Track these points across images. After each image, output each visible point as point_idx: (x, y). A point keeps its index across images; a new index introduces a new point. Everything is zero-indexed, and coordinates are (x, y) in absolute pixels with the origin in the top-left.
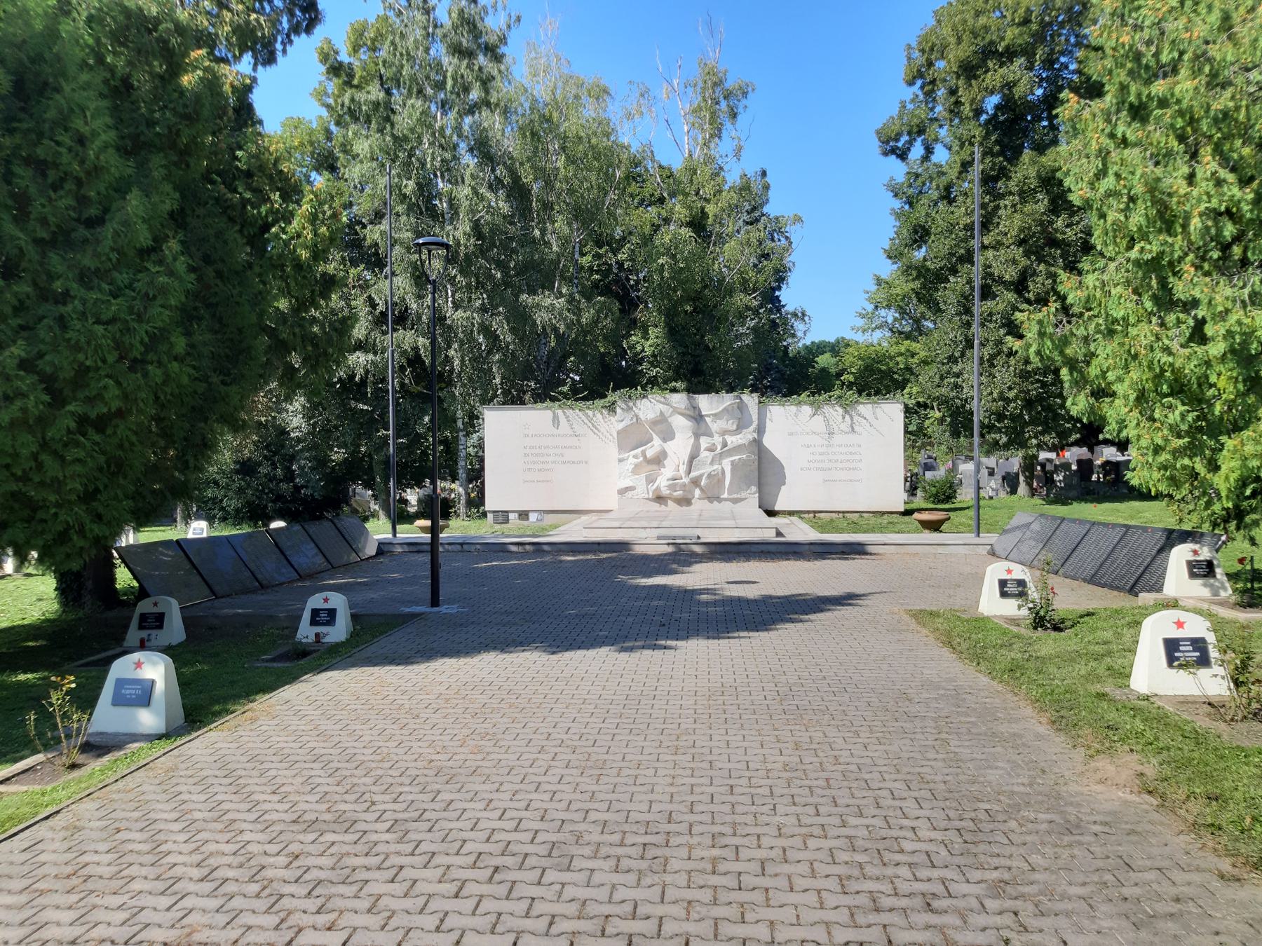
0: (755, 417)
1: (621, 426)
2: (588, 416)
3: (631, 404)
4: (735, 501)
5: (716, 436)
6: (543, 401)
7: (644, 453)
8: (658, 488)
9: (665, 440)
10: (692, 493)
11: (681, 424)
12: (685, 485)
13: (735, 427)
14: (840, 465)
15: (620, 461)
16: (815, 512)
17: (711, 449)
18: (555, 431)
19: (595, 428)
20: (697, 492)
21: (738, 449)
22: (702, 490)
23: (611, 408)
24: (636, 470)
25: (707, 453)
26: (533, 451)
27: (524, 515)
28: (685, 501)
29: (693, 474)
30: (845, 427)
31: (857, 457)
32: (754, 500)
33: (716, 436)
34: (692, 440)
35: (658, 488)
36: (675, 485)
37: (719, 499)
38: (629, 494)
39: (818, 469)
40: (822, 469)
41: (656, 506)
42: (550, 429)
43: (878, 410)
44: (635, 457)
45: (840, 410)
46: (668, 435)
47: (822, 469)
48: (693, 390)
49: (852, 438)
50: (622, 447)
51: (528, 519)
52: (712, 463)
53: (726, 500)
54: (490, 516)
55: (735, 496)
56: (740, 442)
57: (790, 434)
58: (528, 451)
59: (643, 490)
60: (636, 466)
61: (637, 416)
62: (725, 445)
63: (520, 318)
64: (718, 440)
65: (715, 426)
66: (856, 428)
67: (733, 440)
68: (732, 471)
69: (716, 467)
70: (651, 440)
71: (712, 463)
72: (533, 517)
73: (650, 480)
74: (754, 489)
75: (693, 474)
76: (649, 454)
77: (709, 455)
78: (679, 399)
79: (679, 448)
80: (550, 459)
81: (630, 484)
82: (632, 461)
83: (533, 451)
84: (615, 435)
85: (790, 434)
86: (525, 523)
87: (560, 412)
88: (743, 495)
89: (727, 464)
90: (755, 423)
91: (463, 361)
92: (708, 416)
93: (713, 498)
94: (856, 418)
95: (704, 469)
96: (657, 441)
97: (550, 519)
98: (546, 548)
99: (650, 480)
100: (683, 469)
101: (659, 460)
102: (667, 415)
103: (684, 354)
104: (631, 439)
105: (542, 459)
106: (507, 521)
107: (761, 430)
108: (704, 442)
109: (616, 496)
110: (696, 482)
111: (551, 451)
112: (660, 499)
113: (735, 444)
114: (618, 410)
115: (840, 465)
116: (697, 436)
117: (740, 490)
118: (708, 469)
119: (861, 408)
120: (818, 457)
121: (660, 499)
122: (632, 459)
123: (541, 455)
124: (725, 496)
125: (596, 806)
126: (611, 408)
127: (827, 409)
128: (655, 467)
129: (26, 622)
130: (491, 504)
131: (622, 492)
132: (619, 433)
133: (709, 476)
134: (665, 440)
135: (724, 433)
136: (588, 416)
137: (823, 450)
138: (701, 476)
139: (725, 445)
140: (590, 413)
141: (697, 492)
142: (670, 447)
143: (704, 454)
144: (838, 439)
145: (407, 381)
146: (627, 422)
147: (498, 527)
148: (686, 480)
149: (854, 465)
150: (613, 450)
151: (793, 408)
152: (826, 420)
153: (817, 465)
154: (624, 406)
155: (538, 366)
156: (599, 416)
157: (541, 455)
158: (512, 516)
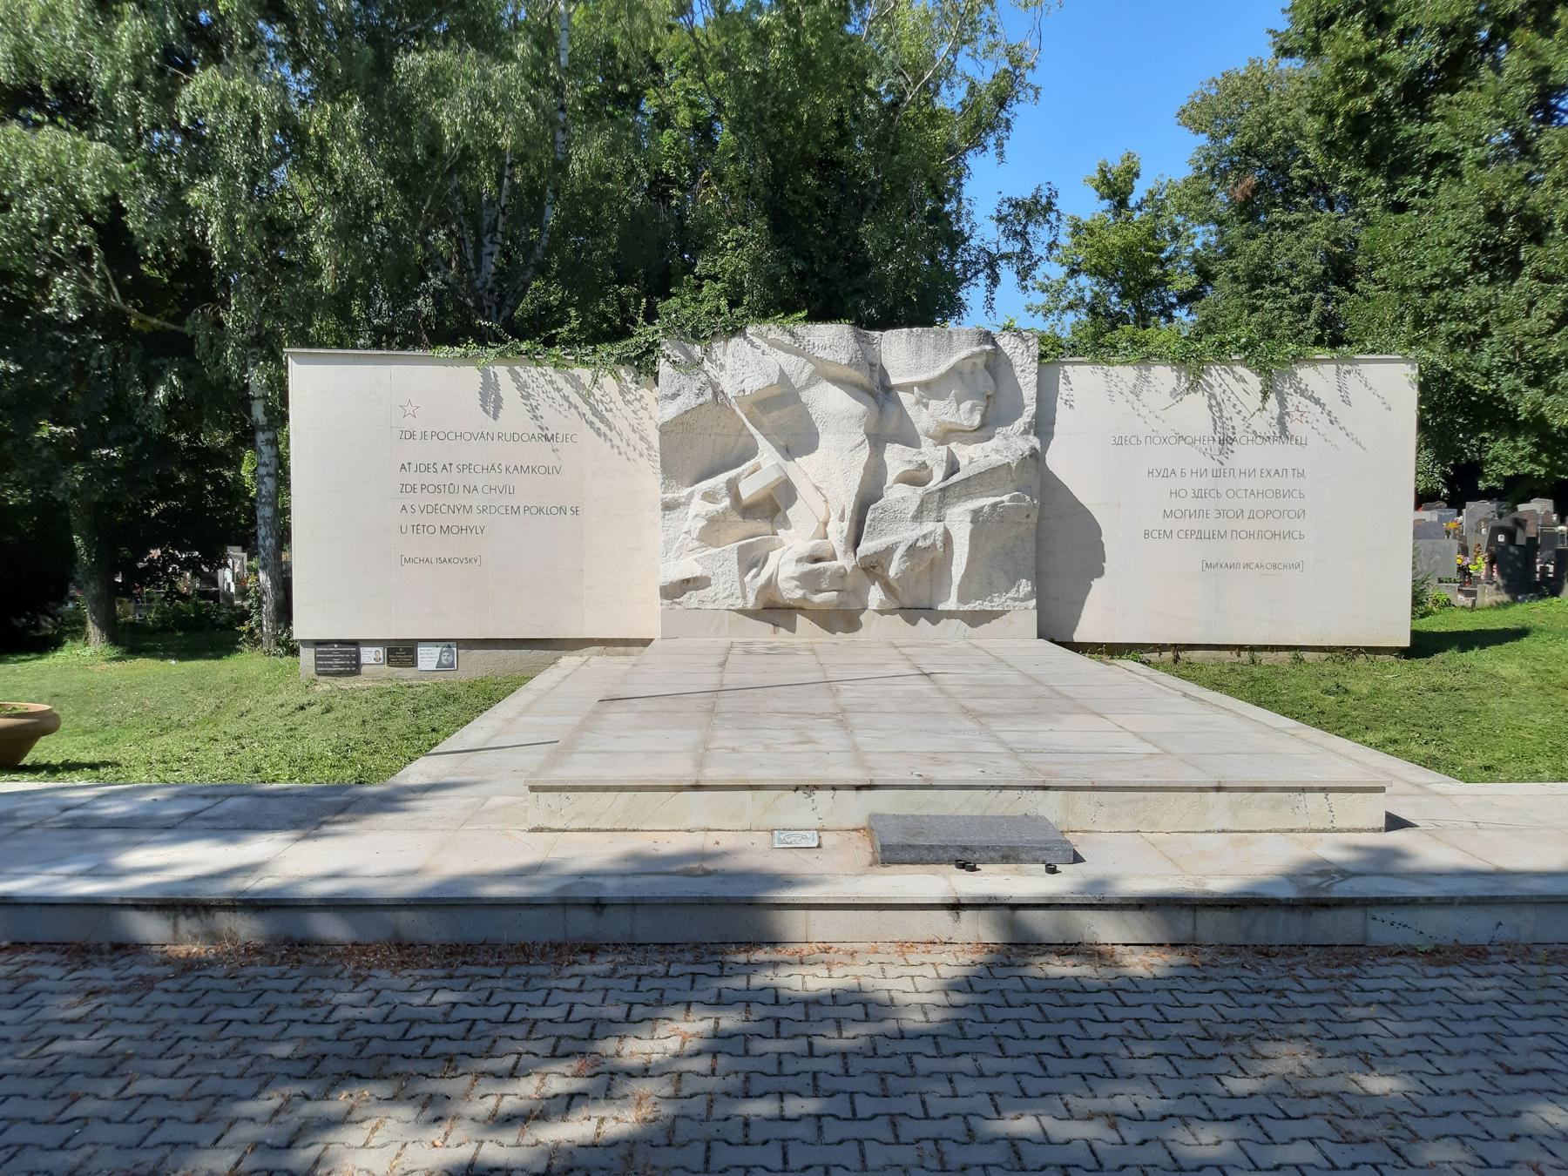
0: (1029, 393)
1: (671, 410)
2: (575, 382)
3: (697, 350)
4: (976, 619)
5: (927, 444)
6: (453, 342)
7: (732, 487)
8: (770, 583)
9: (789, 452)
10: (861, 595)
11: (834, 406)
12: (841, 575)
13: (976, 420)
14: (1243, 524)
15: (668, 507)
16: (1177, 647)
17: (915, 478)
18: (488, 424)
19: (599, 420)
20: (875, 596)
21: (988, 478)
22: (887, 587)
23: (644, 364)
24: (712, 530)
25: (904, 490)
26: (428, 478)
27: (401, 652)
28: (843, 619)
29: (868, 546)
30: (1264, 423)
31: (1294, 504)
32: (1025, 616)
33: (927, 444)
34: (865, 453)
35: (770, 583)
36: (819, 574)
37: (935, 616)
38: (692, 598)
39: (1189, 534)
40: (1200, 535)
41: (763, 633)
42: (478, 420)
43: (1352, 381)
44: (709, 496)
45: (1254, 382)
46: (799, 440)
47: (1200, 535)
48: (866, 324)
49: (1277, 455)
50: (671, 471)
51: (413, 662)
52: (918, 516)
53: (950, 615)
54: (307, 655)
55: (976, 605)
56: (996, 459)
57: (1120, 441)
58: (413, 478)
59: (730, 587)
60: (713, 522)
61: (715, 386)
62: (953, 468)
63: (394, 117)
64: (933, 455)
65: (925, 416)
66: (1292, 427)
67: (974, 456)
68: (974, 537)
69: (928, 526)
70: (750, 452)
71: (918, 516)
72: (428, 658)
73: (751, 560)
74: (1025, 586)
75: (868, 546)
76: (749, 489)
77: (914, 495)
78: (831, 339)
79: (828, 475)
80: (476, 500)
81: (697, 571)
82: (699, 507)
83: (428, 478)
84: (654, 437)
85: (1120, 441)
86: (406, 673)
87: (501, 372)
88: (996, 603)
89: (959, 521)
90: (1030, 409)
91: (229, 222)
92: (908, 388)
93: (917, 610)
94: (1293, 400)
95: (895, 534)
96: (768, 457)
97: (476, 665)
98: (331, 928)
99: (751, 560)
100: (838, 531)
101: (772, 506)
102: (798, 380)
103: (802, 276)
104: (696, 451)
105: (454, 501)
106: (353, 668)
107: (1043, 426)
108: (897, 459)
109: (657, 603)
110: (873, 568)
111: (479, 480)
112: (774, 611)
113: (982, 465)
114: (664, 368)
115: (1243, 524)
116: (877, 441)
117: (989, 588)
118: (906, 534)
119: (1305, 374)
120: (1190, 504)
121: (774, 611)
122: (698, 506)
123: (451, 489)
124: (951, 604)
125: (602, 983)
126: (644, 364)
127: (1217, 376)
128: (762, 526)
129: (1060, 404)
130: (304, 626)
131: (675, 591)
132: (664, 430)
133: (912, 549)
134: (789, 452)
135: (945, 435)
136: (575, 382)
137: (1206, 483)
138: (889, 551)
139: (953, 468)
140: (585, 374)
141: (875, 596)
142: (804, 471)
143: (897, 494)
144: (1246, 455)
145: (94, 287)
146: (687, 400)
147: (325, 685)
148: (845, 562)
149: (1283, 525)
150: (649, 481)
151: (1128, 374)
152: (1215, 406)
153: (1193, 524)
154: (678, 356)
155: (479, 299)
156: (608, 382)
157: (451, 489)
158: (368, 655)
